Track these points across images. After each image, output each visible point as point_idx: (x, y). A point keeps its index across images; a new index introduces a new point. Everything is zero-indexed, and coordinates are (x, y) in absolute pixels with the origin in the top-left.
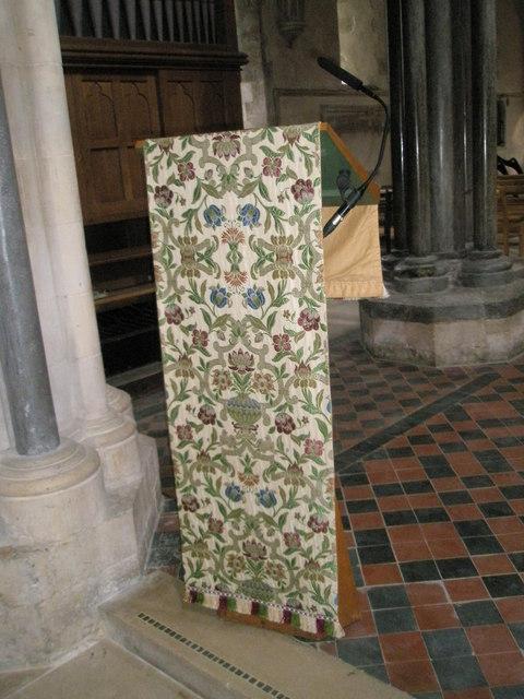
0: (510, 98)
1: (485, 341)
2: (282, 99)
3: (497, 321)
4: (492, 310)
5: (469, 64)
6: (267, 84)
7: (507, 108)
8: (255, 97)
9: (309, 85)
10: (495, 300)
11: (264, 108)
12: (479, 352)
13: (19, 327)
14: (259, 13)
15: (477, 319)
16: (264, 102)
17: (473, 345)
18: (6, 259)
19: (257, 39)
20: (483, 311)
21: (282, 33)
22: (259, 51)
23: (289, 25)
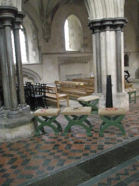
0: (131, 53)
1: (5, 135)
2: (44, 56)
3: (7, 130)
4: (6, 126)
5: (33, 74)
6: (39, 52)
7: (130, 56)
8: (36, 55)
9: (54, 51)
10: (7, 124)
11: (38, 58)
12: (4, 138)
13: (3, 49)
14: (37, 34)
15: (2, 128)
16: (38, 56)
17: (2, 135)
18: (12, 76)
19: (36, 41)
20: (4, 126)
21: (44, 39)
22: (37, 44)
23: (46, 37)
